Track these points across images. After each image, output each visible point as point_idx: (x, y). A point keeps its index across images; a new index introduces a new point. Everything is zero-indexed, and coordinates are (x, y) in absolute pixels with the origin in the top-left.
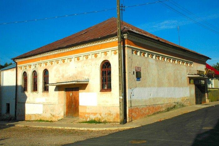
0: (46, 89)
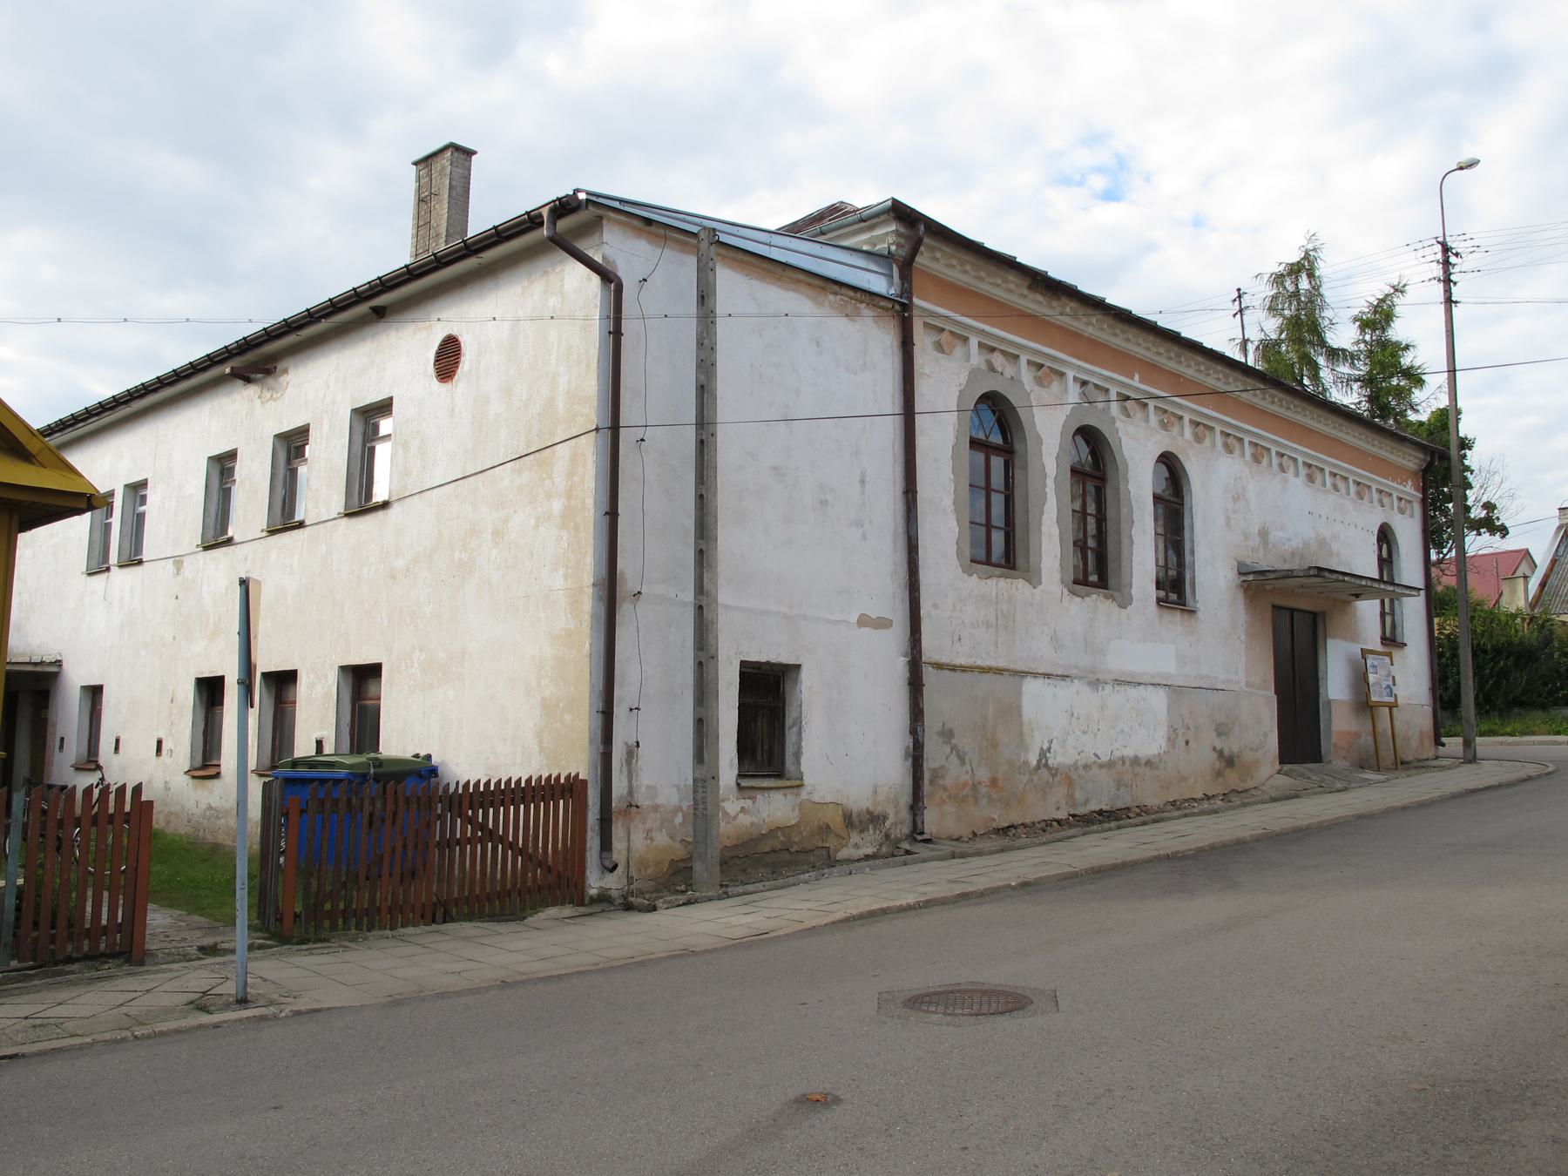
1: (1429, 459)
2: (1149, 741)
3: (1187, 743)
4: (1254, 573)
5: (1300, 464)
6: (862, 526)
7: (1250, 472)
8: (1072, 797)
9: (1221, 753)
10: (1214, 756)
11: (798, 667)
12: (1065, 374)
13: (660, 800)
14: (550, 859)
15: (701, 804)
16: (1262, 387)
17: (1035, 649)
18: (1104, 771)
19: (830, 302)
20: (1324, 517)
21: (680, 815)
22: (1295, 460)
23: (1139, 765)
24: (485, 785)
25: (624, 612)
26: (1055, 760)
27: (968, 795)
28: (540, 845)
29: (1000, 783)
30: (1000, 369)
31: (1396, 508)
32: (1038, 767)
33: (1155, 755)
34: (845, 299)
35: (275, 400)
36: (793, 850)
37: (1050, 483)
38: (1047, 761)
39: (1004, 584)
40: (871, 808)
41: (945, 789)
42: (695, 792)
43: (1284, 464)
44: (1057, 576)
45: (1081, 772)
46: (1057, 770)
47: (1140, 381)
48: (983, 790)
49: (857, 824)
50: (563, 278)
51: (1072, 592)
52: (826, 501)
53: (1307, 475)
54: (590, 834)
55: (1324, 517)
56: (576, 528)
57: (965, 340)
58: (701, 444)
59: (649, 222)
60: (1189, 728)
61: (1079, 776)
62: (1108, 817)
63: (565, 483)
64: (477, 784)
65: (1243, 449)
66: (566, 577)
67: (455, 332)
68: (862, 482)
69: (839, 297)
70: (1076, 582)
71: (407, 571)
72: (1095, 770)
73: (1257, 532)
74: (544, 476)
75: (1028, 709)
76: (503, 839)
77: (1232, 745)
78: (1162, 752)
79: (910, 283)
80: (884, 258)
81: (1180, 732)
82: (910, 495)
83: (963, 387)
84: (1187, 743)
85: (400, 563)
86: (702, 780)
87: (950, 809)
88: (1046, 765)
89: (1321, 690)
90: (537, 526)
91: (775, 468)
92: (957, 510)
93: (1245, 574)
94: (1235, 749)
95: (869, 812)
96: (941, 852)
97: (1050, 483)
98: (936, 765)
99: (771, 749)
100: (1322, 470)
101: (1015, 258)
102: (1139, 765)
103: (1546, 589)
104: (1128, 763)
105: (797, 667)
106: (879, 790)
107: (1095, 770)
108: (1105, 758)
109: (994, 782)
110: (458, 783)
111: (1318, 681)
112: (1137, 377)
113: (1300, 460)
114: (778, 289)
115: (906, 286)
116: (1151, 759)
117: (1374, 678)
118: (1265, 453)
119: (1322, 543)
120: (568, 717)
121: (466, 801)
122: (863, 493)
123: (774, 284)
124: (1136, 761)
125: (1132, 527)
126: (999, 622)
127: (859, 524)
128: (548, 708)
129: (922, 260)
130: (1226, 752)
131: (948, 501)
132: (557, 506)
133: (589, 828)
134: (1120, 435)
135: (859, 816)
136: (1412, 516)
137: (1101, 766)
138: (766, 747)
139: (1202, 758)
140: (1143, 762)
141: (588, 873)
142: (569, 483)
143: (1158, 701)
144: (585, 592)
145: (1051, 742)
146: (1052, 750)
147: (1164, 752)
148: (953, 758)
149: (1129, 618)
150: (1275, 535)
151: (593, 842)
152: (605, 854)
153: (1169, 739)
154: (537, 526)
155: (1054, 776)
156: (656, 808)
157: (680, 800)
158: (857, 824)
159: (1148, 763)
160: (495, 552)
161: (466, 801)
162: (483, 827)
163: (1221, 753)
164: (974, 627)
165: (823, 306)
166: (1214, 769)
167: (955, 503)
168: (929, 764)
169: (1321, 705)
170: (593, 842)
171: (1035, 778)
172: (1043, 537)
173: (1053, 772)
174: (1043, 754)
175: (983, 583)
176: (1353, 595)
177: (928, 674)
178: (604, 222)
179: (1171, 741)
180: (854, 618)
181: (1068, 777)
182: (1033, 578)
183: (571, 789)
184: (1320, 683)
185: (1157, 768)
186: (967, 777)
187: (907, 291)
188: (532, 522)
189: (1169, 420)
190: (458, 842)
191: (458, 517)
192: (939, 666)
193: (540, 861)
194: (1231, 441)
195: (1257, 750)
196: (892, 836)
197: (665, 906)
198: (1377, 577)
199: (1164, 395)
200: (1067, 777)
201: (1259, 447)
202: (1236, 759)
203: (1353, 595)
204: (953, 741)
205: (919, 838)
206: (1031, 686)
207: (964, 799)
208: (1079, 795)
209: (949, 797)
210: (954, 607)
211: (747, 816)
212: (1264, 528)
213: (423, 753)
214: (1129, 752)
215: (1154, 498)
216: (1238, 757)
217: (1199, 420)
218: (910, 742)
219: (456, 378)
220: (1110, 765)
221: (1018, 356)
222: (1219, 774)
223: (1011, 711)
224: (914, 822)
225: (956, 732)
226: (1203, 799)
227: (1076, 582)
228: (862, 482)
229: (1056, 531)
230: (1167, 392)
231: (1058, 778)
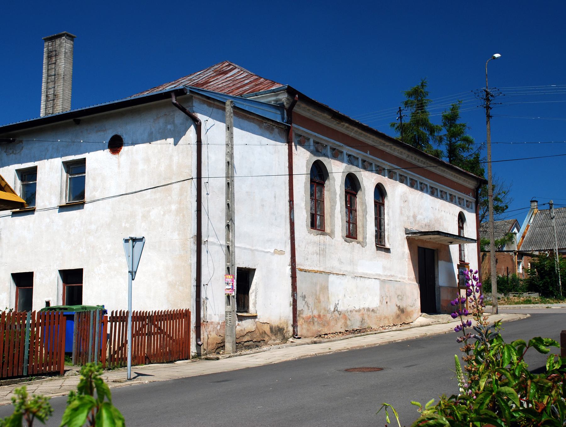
0: (314, 323)
1: (479, 184)
2: (373, 301)
3: (387, 303)
4: (412, 233)
5: (428, 187)
6: (275, 214)
7: (410, 190)
8: (346, 323)
9: (399, 307)
10: (397, 308)
11: (255, 270)
12: (343, 152)
13: (213, 320)
14: (43, 360)
15: (229, 321)
16: (436, 165)
17: (332, 264)
18: (357, 313)
19: (264, 126)
20: (451, 214)
21: (219, 326)
22: (426, 185)
23: (369, 311)
24: (154, 313)
25: (203, 247)
26: (340, 308)
27: (311, 320)
28: (44, 352)
29: (322, 317)
30: (320, 151)
31: (465, 205)
32: (334, 311)
33: (375, 308)
34: (269, 125)
35: (15, 154)
36: (254, 341)
37: (338, 196)
38: (337, 308)
39: (322, 237)
40: (279, 325)
41: (303, 319)
42: (226, 316)
43: (422, 187)
44: (340, 234)
45: (349, 313)
46: (341, 312)
47: (370, 154)
48: (316, 319)
49: (274, 331)
50: (174, 118)
51: (346, 241)
52: (264, 205)
53: (431, 191)
54: (191, 332)
55: (451, 214)
56: (184, 216)
57: (309, 139)
58: (228, 185)
59: (208, 98)
60: (387, 297)
61: (349, 315)
62: (360, 332)
63: (177, 198)
64: (174, 311)
65: (407, 181)
66: (179, 234)
67: (119, 134)
68: (275, 197)
69: (267, 124)
70: (347, 237)
71: (96, 230)
72: (354, 312)
73: (412, 215)
74: (167, 195)
75: (331, 289)
76: (166, 333)
77: (403, 305)
78: (378, 306)
79: (291, 118)
80: (279, 107)
81: (384, 298)
82: (291, 202)
83: (308, 159)
84: (387, 303)
85: (93, 227)
86: (229, 312)
87: (305, 326)
88: (337, 310)
89: (436, 283)
90: (164, 215)
91: (247, 192)
92: (306, 208)
93: (408, 233)
94: (404, 306)
95: (278, 327)
96: (121, 384)
97: (338, 196)
98: (300, 309)
99: (244, 302)
100: (437, 189)
101: (328, 106)
102: (369, 311)
103: (525, 239)
104: (366, 310)
105: (254, 270)
106: (281, 318)
107: (354, 312)
108: (357, 308)
109: (319, 316)
110: (152, 311)
111: (435, 278)
112: (368, 153)
113: (428, 185)
114: (248, 122)
115: (290, 119)
116: (374, 308)
117: (462, 277)
118: (415, 182)
119: (437, 220)
120: (181, 288)
121: (155, 318)
122: (275, 201)
123: (246, 120)
124: (368, 310)
125: (366, 214)
126: (321, 252)
127: (273, 214)
128: (171, 285)
129: (296, 109)
130: (401, 307)
131: (303, 205)
132: (174, 207)
133: (191, 330)
134: (362, 176)
135: (275, 328)
136: (472, 208)
137: (356, 311)
138: (243, 301)
139: (392, 310)
140: (371, 310)
141: (191, 347)
142: (180, 198)
143: (376, 284)
144: (188, 241)
145: (339, 301)
146: (339, 304)
147: (379, 306)
148: (306, 306)
149: (365, 251)
150: (419, 217)
151: (193, 335)
152: (198, 340)
153: (380, 301)
154: (164, 215)
155: (340, 315)
156: (212, 323)
157: (219, 320)
158: (274, 331)
159: (373, 310)
160: (143, 224)
161: (155, 318)
162: (160, 328)
163: (399, 307)
164: (312, 255)
165: (262, 128)
166: (396, 314)
167: (306, 205)
168: (299, 308)
169: (436, 289)
170: (193, 335)
171: (333, 315)
172: (335, 218)
173: (340, 313)
174: (336, 306)
175: (315, 237)
176: (449, 242)
177: (298, 274)
178: (193, 98)
179: (381, 302)
180: (272, 251)
181: (345, 315)
182: (331, 235)
183: (186, 314)
184: (436, 279)
185: (376, 313)
186: (311, 314)
187: (290, 121)
188: (162, 213)
189: (351, 160)
190: (147, 334)
191: (124, 210)
192: (301, 270)
193: (48, 363)
194: (402, 180)
195: (412, 307)
196: (286, 337)
197: (222, 358)
198: (457, 233)
199: (399, 168)
200: (344, 316)
201: (423, 184)
202: (404, 310)
203: (449, 242)
204: (306, 300)
205: (296, 337)
206: (332, 278)
207: (310, 323)
208: (349, 323)
209: (305, 322)
210: (305, 246)
211: (240, 327)
212: (415, 214)
213: (101, 304)
214: (366, 306)
215: (384, 205)
216: (405, 309)
217: (402, 174)
218: (291, 300)
219: (120, 153)
220: (359, 311)
221: (358, 158)
222: (398, 316)
223: (325, 288)
224: (294, 331)
225: (306, 296)
226: (393, 326)
227: (347, 237)
228: (275, 197)
229: (340, 216)
230: (401, 167)
231: (341, 316)
